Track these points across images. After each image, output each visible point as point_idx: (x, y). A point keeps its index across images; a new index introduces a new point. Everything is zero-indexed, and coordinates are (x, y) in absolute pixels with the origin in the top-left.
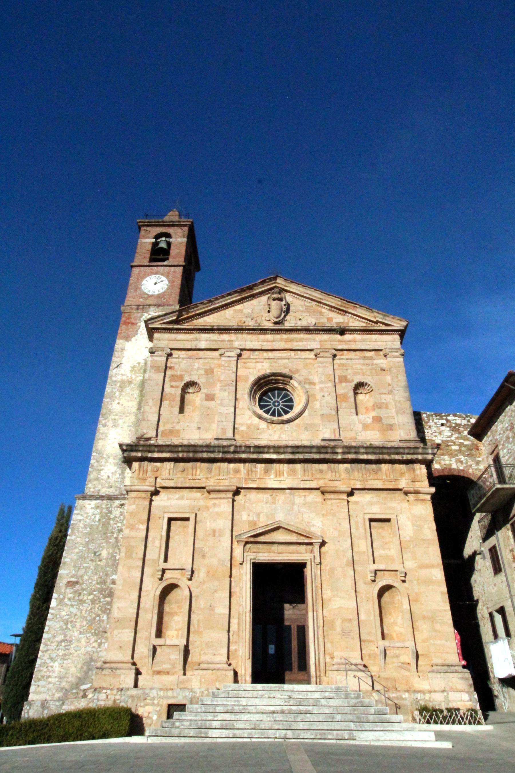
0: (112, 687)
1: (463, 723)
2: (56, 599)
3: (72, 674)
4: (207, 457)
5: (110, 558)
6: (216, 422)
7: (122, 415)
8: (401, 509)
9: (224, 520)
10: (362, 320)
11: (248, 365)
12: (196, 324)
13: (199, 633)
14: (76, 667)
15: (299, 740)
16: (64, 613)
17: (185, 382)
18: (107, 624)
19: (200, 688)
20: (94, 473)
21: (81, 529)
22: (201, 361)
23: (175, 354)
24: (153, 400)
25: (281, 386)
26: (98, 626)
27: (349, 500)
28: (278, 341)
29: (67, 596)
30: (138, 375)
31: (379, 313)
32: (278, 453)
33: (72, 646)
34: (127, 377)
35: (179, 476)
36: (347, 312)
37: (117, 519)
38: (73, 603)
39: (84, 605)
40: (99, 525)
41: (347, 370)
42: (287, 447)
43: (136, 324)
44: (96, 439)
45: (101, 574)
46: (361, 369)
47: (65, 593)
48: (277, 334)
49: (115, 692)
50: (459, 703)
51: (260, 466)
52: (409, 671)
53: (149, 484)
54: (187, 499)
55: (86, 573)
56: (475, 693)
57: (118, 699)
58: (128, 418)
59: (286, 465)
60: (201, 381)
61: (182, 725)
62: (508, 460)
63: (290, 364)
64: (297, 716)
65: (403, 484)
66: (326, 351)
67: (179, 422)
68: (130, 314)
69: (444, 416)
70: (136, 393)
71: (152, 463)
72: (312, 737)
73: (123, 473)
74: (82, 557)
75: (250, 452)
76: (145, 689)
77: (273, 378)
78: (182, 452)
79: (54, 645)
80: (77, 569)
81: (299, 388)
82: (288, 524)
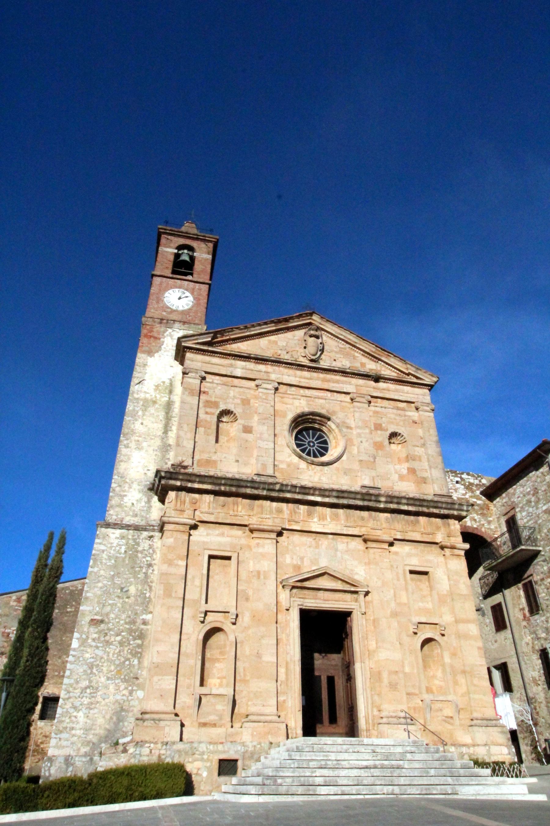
0: (156, 740)
1: (510, 776)
2: (77, 639)
3: (100, 726)
4: (251, 493)
5: (139, 596)
6: (255, 456)
7: (147, 437)
8: (438, 563)
9: (269, 562)
10: (393, 369)
11: (285, 400)
12: (230, 349)
13: (245, 681)
14: (104, 717)
15: (410, 796)
16: (87, 655)
17: (221, 409)
18: (138, 669)
19: (252, 742)
20: (116, 499)
21: (104, 561)
22: (237, 389)
23: (209, 378)
24: (188, 425)
25: (316, 426)
26: (128, 671)
27: (191, 533)
28: (316, 380)
29: (90, 636)
30: (163, 395)
31: (412, 366)
32: (324, 496)
33: (99, 693)
34: (151, 395)
35: (220, 510)
36: (380, 360)
37: (146, 552)
38: (99, 645)
39: (111, 646)
40: (125, 557)
41: (382, 418)
42: (333, 490)
43: (160, 339)
44: (117, 461)
45: (130, 613)
46: (395, 419)
47: (88, 632)
48: (314, 372)
49: (159, 746)
50: (499, 756)
51: (303, 508)
52: (452, 724)
53: (187, 517)
54: (227, 536)
55: (112, 611)
56: (513, 746)
57: (164, 755)
58: (153, 441)
59: (328, 509)
60: (238, 411)
61: (285, 782)
62: (527, 522)
63: (327, 405)
64: (394, 771)
65: (439, 538)
66: (362, 396)
67: (215, 452)
68: (152, 327)
69: (459, 474)
70: (162, 415)
71: (190, 494)
72: (418, 792)
73: (149, 501)
74: (107, 593)
75: (295, 492)
76: (192, 742)
77: (311, 417)
78: (225, 485)
79: (78, 691)
80: (101, 606)
81: (337, 430)
82: (334, 571)
